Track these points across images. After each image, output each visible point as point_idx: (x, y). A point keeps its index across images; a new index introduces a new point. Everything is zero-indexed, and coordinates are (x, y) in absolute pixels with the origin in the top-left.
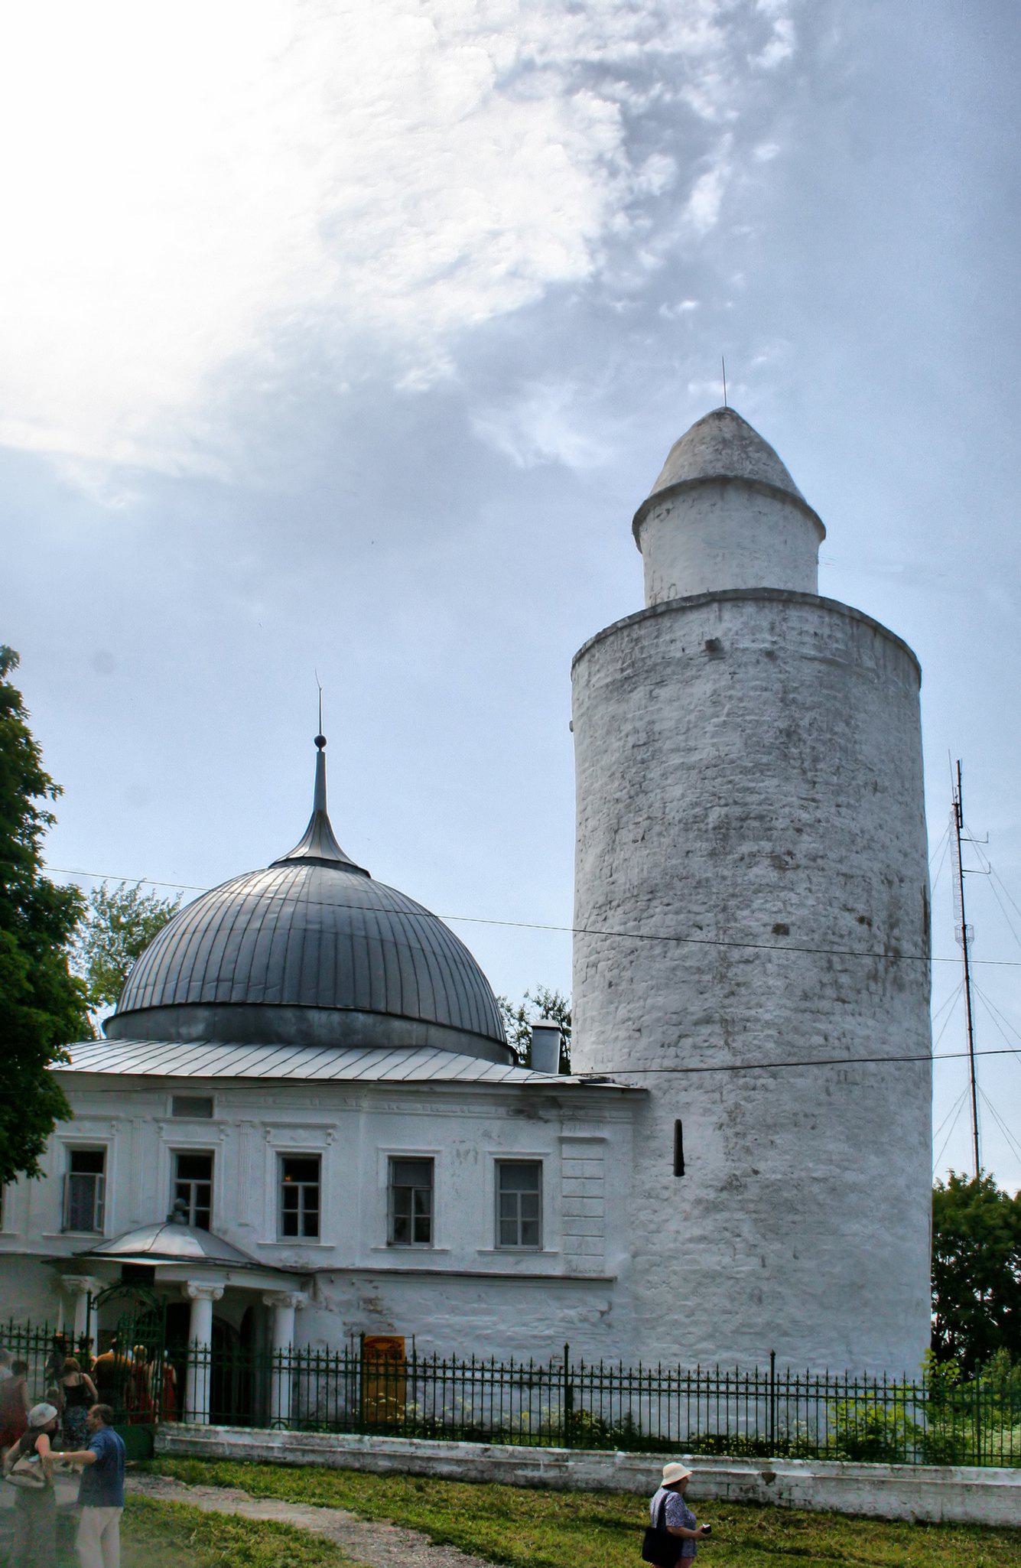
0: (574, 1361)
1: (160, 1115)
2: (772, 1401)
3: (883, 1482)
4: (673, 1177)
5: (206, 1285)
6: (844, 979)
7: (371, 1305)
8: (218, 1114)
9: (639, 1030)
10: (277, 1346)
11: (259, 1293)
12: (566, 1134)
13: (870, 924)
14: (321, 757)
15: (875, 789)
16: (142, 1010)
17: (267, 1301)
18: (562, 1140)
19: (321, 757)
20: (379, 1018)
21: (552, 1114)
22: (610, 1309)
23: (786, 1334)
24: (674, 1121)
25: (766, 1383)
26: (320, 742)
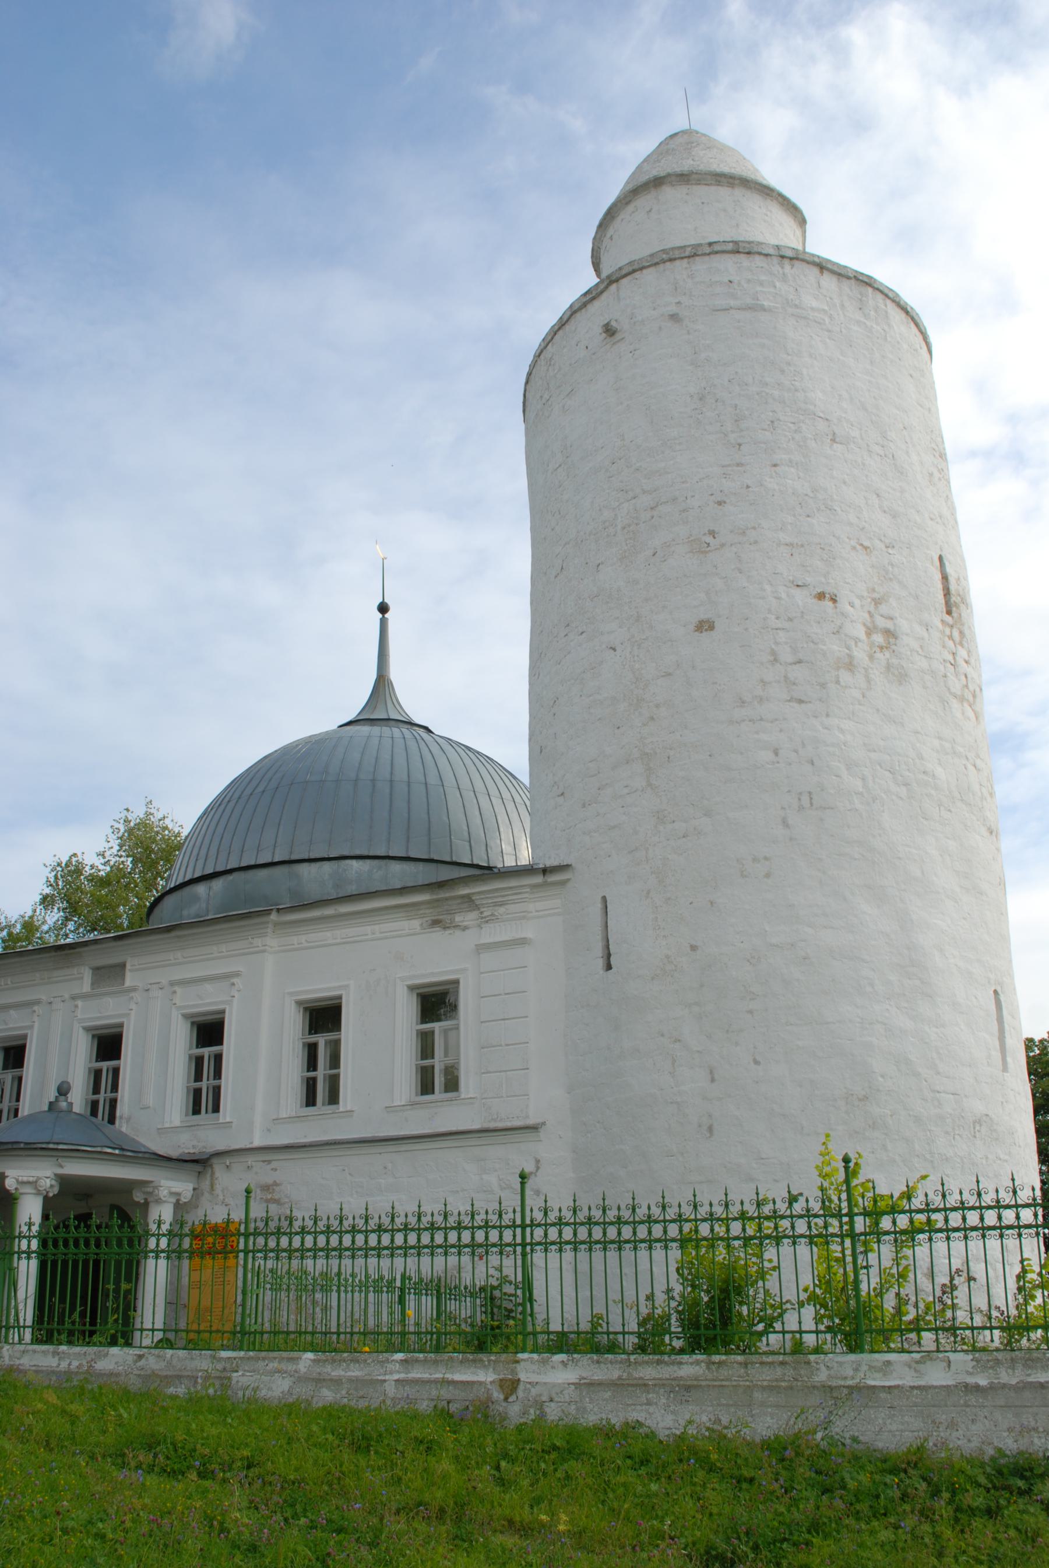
2: (524, 1255)
3: (688, 1388)
4: (601, 972)
6: (798, 673)
9: (562, 794)
11: (127, 1187)
12: (486, 939)
13: (834, 600)
15: (833, 440)
17: (138, 1197)
18: (481, 948)
20: (376, 862)
21: (469, 918)
22: (538, 1168)
24: (599, 899)
25: (514, 1226)
26: (383, 608)
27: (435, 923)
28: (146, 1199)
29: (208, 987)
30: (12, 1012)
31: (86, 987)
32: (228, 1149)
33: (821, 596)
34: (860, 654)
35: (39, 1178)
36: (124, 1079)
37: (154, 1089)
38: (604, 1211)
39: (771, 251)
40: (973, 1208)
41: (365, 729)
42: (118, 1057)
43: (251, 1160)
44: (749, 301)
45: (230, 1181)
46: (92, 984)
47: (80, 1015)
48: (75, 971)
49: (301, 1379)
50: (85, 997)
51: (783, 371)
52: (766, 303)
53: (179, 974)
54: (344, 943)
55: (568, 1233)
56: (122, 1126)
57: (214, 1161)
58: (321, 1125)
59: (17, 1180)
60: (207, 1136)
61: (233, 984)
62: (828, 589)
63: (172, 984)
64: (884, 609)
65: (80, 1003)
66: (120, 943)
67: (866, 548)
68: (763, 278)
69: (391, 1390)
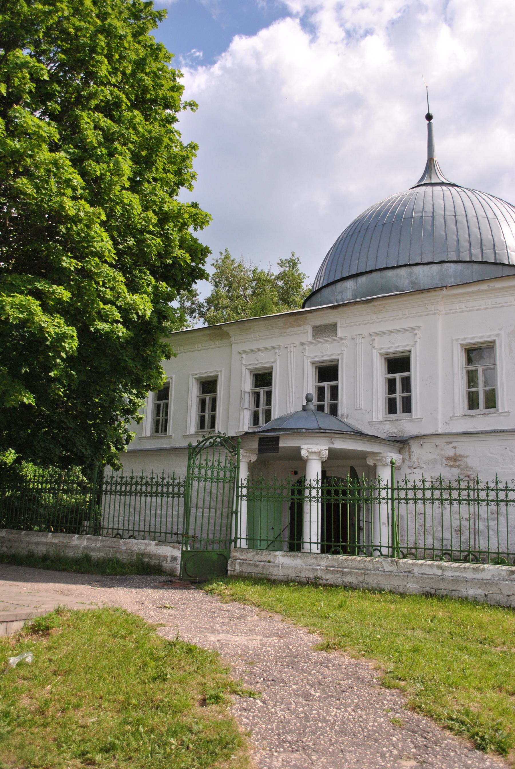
1: (304, 340)
7: (454, 460)
8: (340, 333)
10: (308, 478)
11: (363, 456)
14: (430, 126)
17: (370, 462)
19: (430, 126)
20: (465, 265)
26: (429, 117)
28: (374, 464)
30: (261, 353)
31: (310, 338)
32: (419, 434)
35: (321, 450)
36: (275, 400)
37: (363, 397)
38: (406, 483)
40: (493, 490)
41: (423, 188)
42: (168, 399)
43: (438, 441)
46: (313, 336)
47: (307, 354)
48: (302, 328)
50: (309, 344)
53: (375, 329)
54: (494, 307)
55: (492, 495)
57: (411, 441)
58: (483, 421)
59: (308, 451)
60: (407, 426)
61: (416, 334)
63: (371, 335)
65: (307, 347)
66: (335, 311)
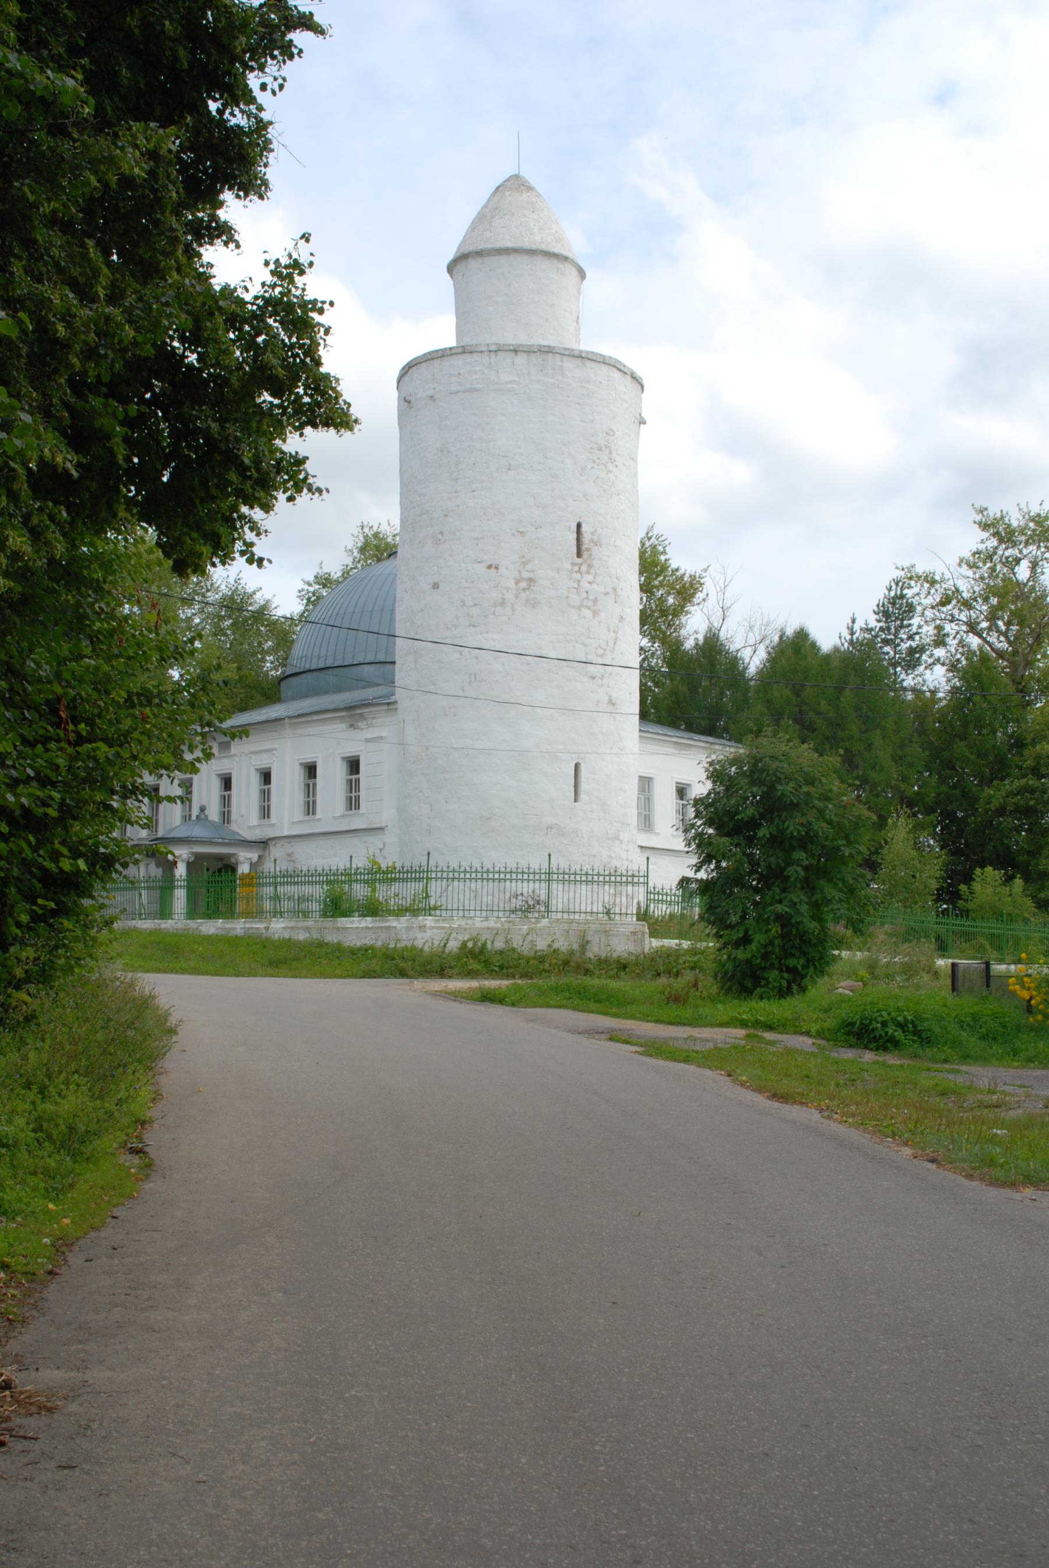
0: (554, 865)
5: (249, 855)
6: (474, 611)
11: (229, 856)
12: (369, 736)
13: (497, 568)
16: (310, 671)
17: (233, 861)
18: (368, 740)
23: (442, 854)
27: (352, 726)
29: (265, 755)
33: (490, 567)
34: (509, 597)
39: (484, 349)
44: (468, 386)
45: (276, 852)
49: (217, 929)
51: (483, 430)
52: (477, 386)
56: (234, 827)
62: (494, 562)
63: (251, 753)
64: (529, 567)
67: (521, 533)
68: (478, 368)
69: (238, 931)
